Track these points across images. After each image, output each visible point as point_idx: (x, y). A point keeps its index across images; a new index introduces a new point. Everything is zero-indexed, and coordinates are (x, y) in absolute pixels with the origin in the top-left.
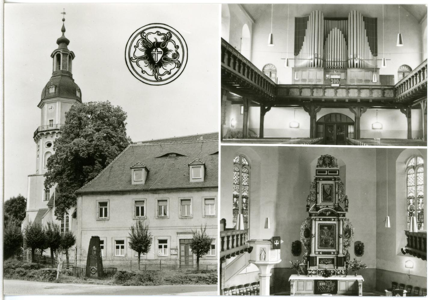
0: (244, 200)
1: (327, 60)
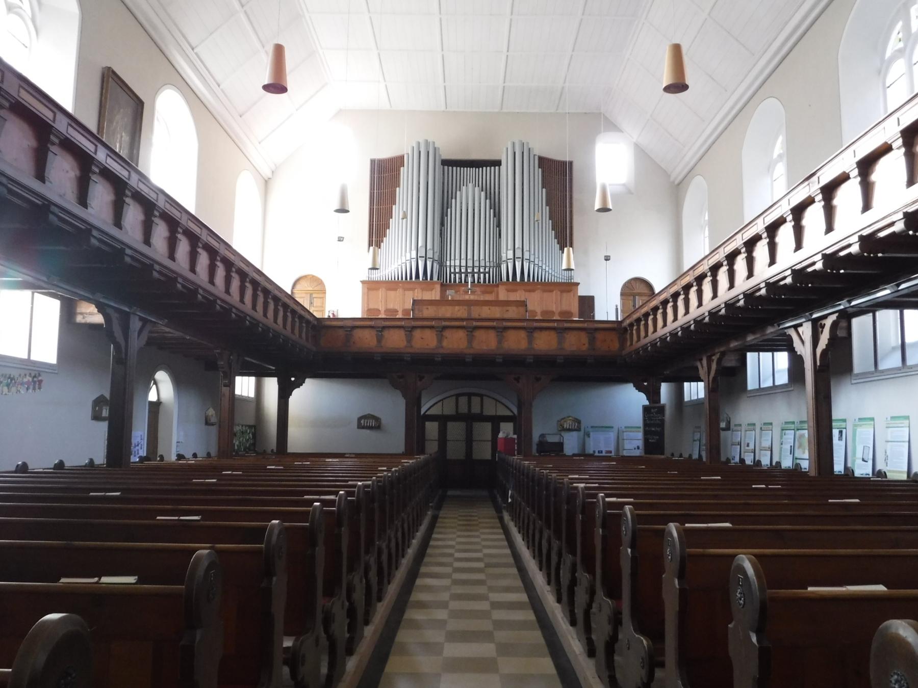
1: (448, 263)
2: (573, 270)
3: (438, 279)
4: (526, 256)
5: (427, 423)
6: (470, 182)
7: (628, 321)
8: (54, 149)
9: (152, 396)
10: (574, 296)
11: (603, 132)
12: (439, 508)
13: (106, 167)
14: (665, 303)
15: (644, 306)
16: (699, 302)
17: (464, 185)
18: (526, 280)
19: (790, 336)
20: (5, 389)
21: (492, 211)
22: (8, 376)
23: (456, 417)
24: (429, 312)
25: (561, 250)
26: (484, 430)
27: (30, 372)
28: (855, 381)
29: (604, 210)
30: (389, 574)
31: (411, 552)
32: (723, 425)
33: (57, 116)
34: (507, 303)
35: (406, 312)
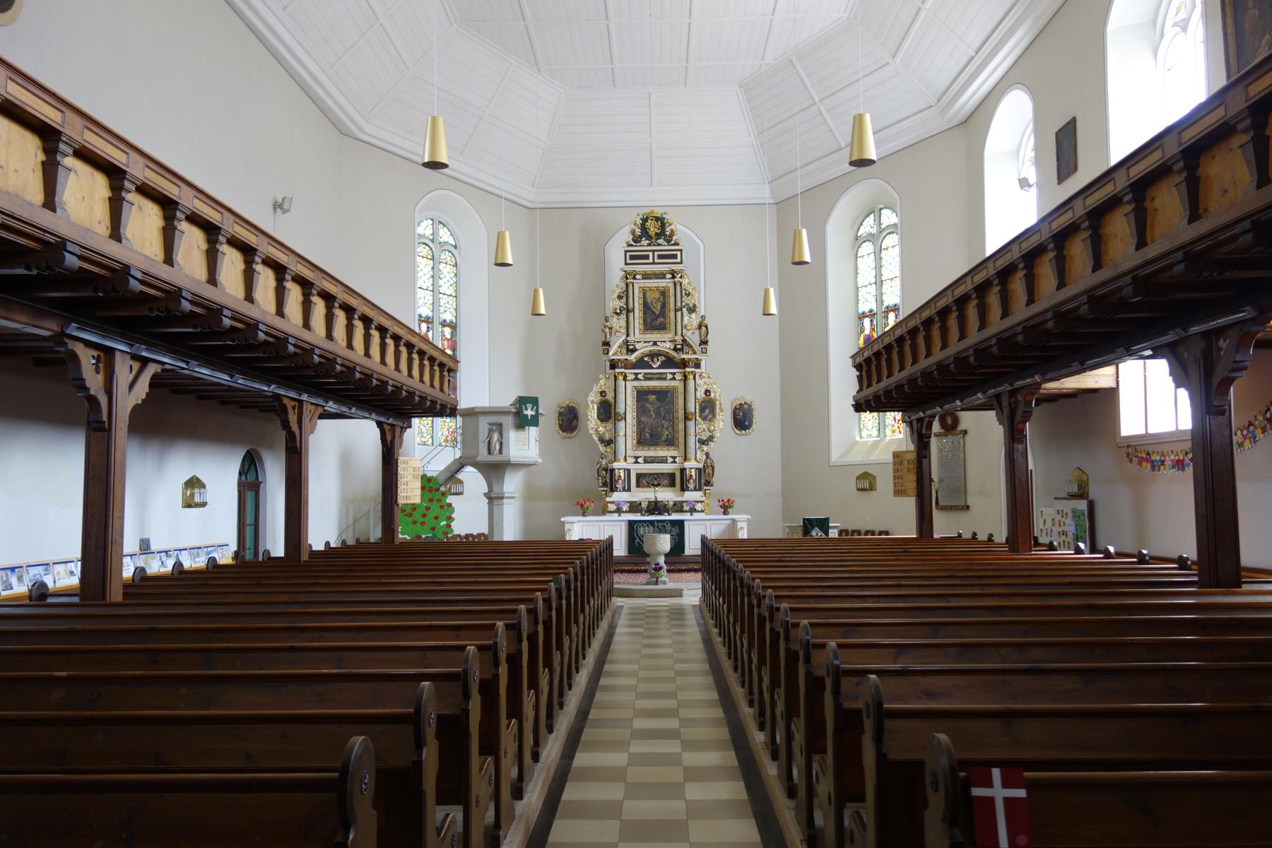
0: (447, 331)
8: (70, 161)
16: (960, 333)
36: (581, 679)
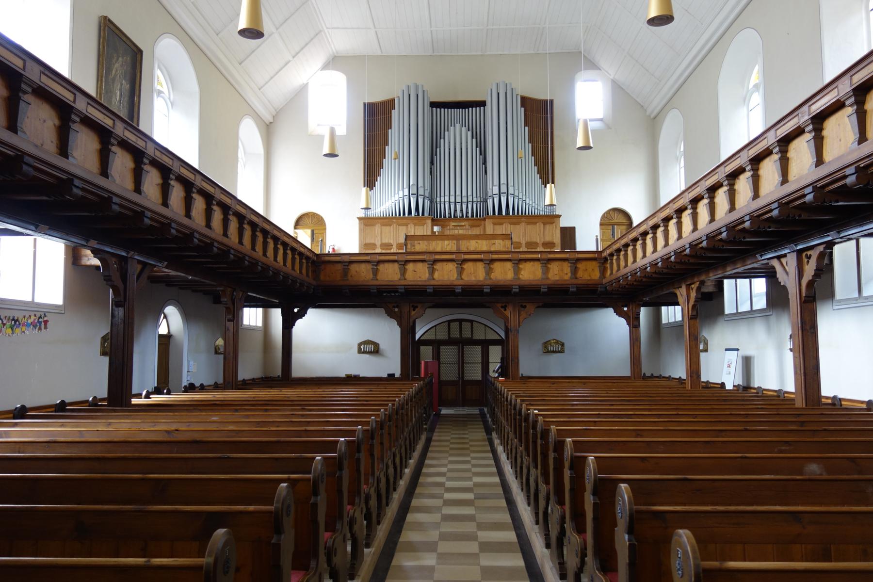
1: (438, 200)
2: (555, 205)
3: (429, 215)
4: (511, 191)
5: (422, 348)
6: (457, 123)
7: (608, 252)
8: (28, 98)
9: (163, 330)
10: (556, 227)
11: (584, 70)
12: (432, 430)
13: (87, 116)
14: (645, 234)
15: (624, 237)
17: (451, 126)
18: (511, 214)
19: (774, 268)
20: (9, 331)
21: (478, 149)
22: (11, 318)
23: (450, 342)
24: (420, 246)
25: (543, 184)
26: (474, 353)
27: (35, 313)
28: (837, 307)
29: (587, 148)
30: (387, 498)
31: (403, 484)
32: (701, 347)
33: (27, 63)
34: (494, 237)
35: (399, 246)
36: (397, 497)
